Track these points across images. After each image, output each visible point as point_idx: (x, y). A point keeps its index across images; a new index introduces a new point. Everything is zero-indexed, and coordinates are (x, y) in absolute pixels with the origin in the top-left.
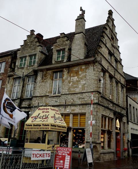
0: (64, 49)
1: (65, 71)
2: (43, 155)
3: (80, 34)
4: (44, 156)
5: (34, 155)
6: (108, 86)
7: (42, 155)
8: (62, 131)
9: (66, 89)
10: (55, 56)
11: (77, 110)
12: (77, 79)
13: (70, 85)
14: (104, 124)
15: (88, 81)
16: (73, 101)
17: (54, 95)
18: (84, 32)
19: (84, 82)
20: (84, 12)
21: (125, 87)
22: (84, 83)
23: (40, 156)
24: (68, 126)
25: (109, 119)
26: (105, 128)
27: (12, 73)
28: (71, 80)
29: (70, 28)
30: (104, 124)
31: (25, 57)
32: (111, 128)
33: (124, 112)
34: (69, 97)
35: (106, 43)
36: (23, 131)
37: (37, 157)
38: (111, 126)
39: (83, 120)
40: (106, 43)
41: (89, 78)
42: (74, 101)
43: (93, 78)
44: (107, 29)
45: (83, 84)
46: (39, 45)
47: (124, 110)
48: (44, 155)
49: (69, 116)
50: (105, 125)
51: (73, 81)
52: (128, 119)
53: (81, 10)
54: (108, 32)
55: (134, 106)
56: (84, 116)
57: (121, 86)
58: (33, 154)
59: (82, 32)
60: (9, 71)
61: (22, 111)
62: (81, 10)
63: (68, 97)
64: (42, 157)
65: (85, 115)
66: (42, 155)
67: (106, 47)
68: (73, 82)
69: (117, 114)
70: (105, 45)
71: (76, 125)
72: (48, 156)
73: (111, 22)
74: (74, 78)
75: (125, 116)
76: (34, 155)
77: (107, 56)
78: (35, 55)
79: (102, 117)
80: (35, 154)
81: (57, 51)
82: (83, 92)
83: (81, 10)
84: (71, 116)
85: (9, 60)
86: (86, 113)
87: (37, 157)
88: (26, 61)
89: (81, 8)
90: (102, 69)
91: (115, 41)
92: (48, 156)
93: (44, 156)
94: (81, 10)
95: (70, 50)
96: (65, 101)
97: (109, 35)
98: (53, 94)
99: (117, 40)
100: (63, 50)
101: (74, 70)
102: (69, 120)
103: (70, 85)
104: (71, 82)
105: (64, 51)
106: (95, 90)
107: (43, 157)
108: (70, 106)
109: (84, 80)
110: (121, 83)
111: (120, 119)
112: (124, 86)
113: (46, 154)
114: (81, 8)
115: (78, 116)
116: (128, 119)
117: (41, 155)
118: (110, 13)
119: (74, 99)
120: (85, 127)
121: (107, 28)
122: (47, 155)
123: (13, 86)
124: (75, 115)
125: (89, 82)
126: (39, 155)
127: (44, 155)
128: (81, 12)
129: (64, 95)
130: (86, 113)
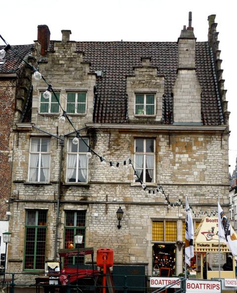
13: (175, 168)
15: (210, 165)
19: (204, 167)
28: (177, 160)
41: (212, 161)
45: (201, 170)
101: (182, 140)
103: (175, 168)
104: (178, 163)
125: (212, 167)
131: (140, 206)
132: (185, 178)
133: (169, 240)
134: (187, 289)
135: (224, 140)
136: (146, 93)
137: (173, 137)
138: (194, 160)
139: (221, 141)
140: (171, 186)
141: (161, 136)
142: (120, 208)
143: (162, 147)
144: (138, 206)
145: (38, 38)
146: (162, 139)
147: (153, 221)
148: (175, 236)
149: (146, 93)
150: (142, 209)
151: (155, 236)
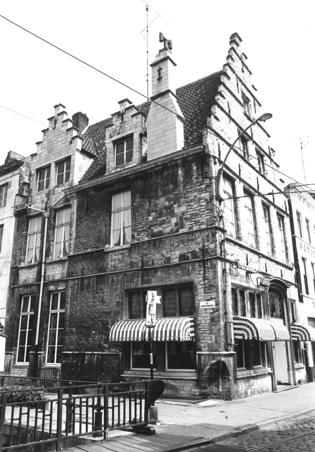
0: (132, 135)
6: (245, 215)
8: (179, 158)
12: (167, 204)
13: (151, 218)
17: (118, 248)
20: (167, 44)
21: (287, 215)
22: (183, 210)
29: (140, 91)
31: (48, 167)
33: (289, 276)
35: (229, 112)
36: (129, 152)
40: (229, 112)
41: (193, 198)
44: (229, 78)
47: (288, 271)
52: (300, 291)
53: (161, 41)
55: (308, 218)
57: (278, 214)
61: (160, 53)
62: (161, 41)
67: (231, 119)
70: (229, 115)
75: (292, 284)
83: (163, 39)
89: (161, 34)
91: (253, 106)
94: (163, 39)
97: (235, 92)
98: (116, 245)
99: (257, 104)
103: (151, 218)
105: (130, 142)
110: (276, 207)
112: (285, 212)
114: (161, 34)
116: (300, 291)
118: (235, 39)
121: (229, 72)
123: (28, 236)
128: (161, 46)
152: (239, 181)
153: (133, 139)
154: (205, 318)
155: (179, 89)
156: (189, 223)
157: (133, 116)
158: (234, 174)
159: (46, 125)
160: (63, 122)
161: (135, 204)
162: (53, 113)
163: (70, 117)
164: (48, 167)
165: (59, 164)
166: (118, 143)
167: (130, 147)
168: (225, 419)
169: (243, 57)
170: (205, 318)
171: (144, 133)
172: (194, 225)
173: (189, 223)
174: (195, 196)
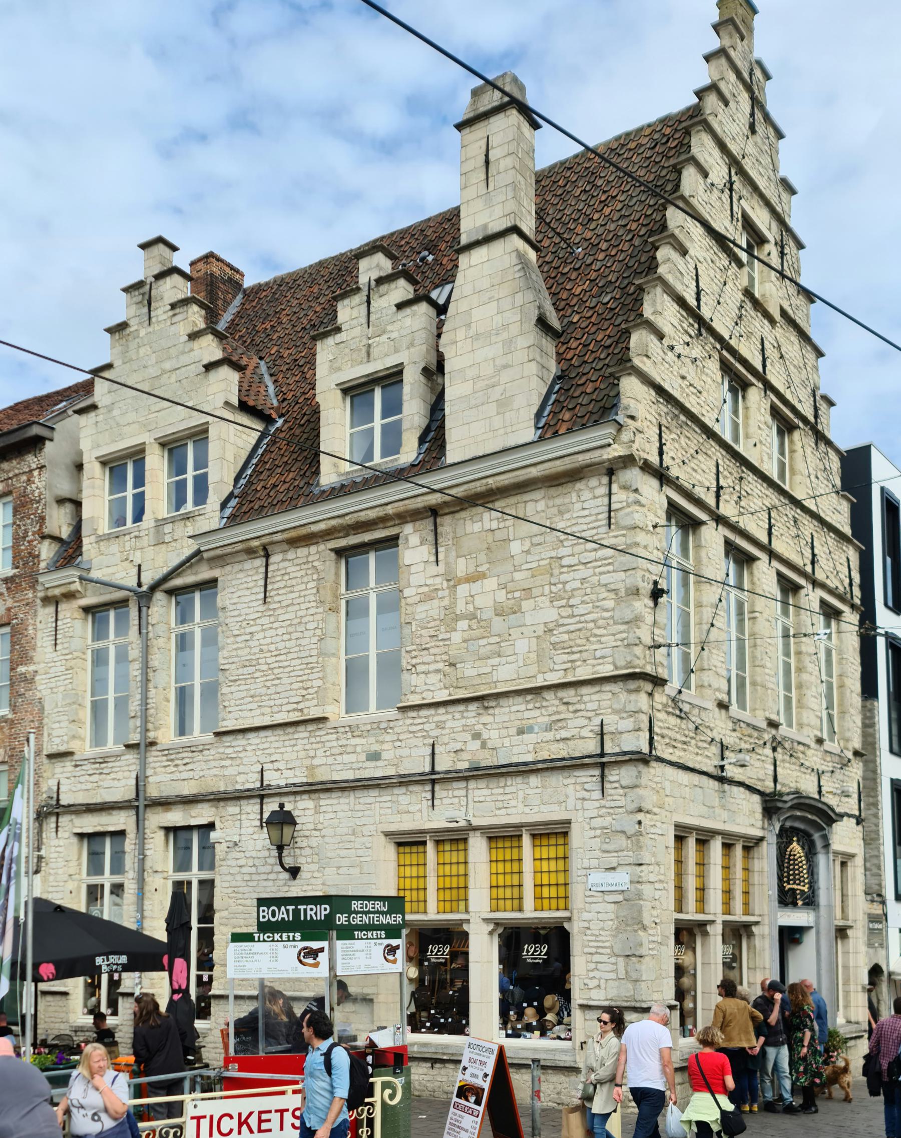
1: (414, 540)
2: (260, 1121)
3: (498, 248)
4: (264, 1126)
5: (205, 1123)
7: (253, 1121)
9: (432, 667)
10: (337, 430)
11: (524, 802)
13: (456, 637)
14: (691, 883)
15: (572, 602)
16: (484, 745)
18: (528, 225)
19: (550, 614)
23: (240, 1125)
24: (868, 704)
25: (727, 847)
26: (703, 912)
27: (70, 575)
28: (460, 607)
30: (691, 883)
31: (137, 455)
32: (746, 904)
34: (455, 721)
37: (225, 1131)
38: (746, 893)
39: (553, 867)
41: (577, 584)
42: (490, 744)
43: (605, 579)
45: (540, 630)
46: (218, 355)
48: (264, 1117)
49: (461, 847)
50: (702, 890)
51: (471, 607)
54: (704, 187)
56: (561, 841)
58: (198, 1119)
59: (515, 230)
60: (43, 565)
63: (449, 724)
64: (251, 1132)
65: (566, 834)
66: (253, 1121)
68: (472, 617)
69: (792, 808)
70: (694, 314)
71: (509, 903)
72: (293, 1125)
73: (744, 97)
74: (476, 587)
76: (205, 1123)
77: (708, 394)
78: (200, 435)
79: (680, 839)
80: (211, 1117)
81: (345, 391)
82: (540, 682)
84: (478, 846)
85: (29, 481)
86: (569, 822)
87: (225, 1131)
88: (143, 485)
90: (673, 510)
92: (293, 1125)
93: (264, 1126)
95: (435, 371)
96: (429, 751)
100: (392, 378)
101: (477, 527)
102: (462, 872)
103: (456, 637)
104: (463, 617)
106: (621, 663)
107: (260, 1131)
108: (462, 784)
109: (544, 601)
111: (816, 836)
113: (282, 1112)
115: (520, 847)
117: (246, 1122)
119: (485, 736)
120: (565, 914)
122: (288, 1116)
124: (503, 837)
125: (582, 609)
126: (234, 1124)
127: (264, 1117)
129: (424, 712)
130: (569, 822)
131: (352, 794)
132: (489, 670)
133: (554, 906)
134: (486, 1086)
135: (625, 487)
136: (189, 437)
137: (447, 524)
138: (517, 594)
139: (610, 494)
140: (442, 710)
141: (408, 529)
142: (282, 806)
143: (413, 569)
144: (346, 793)
145: (258, 289)
146: (414, 540)
147: (399, 844)
148: (516, 890)
149: (189, 437)
150: (356, 798)
151: (546, 893)
152: (715, 525)
153: (402, 381)
154: (601, 916)
155: (467, 939)
156: (565, 658)
157: (400, 306)
158: (699, 503)
159: (121, 308)
160: (173, 306)
161: (459, 984)
162: (139, 268)
163: (182, 261)
164: (137, 455)
165: (173, 446)
166: (356, 392)
167: (393, 407)
168: (302, 875)
169: (753, 79)
170: (601, 916)
171: (434, 367)
172: (578, 663)
173: (565, 658)
174: (583, 580)
